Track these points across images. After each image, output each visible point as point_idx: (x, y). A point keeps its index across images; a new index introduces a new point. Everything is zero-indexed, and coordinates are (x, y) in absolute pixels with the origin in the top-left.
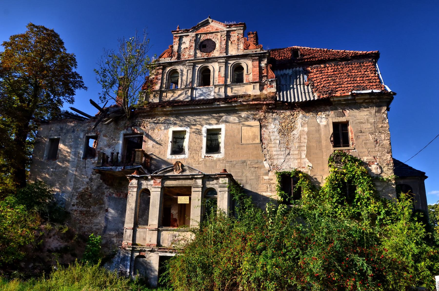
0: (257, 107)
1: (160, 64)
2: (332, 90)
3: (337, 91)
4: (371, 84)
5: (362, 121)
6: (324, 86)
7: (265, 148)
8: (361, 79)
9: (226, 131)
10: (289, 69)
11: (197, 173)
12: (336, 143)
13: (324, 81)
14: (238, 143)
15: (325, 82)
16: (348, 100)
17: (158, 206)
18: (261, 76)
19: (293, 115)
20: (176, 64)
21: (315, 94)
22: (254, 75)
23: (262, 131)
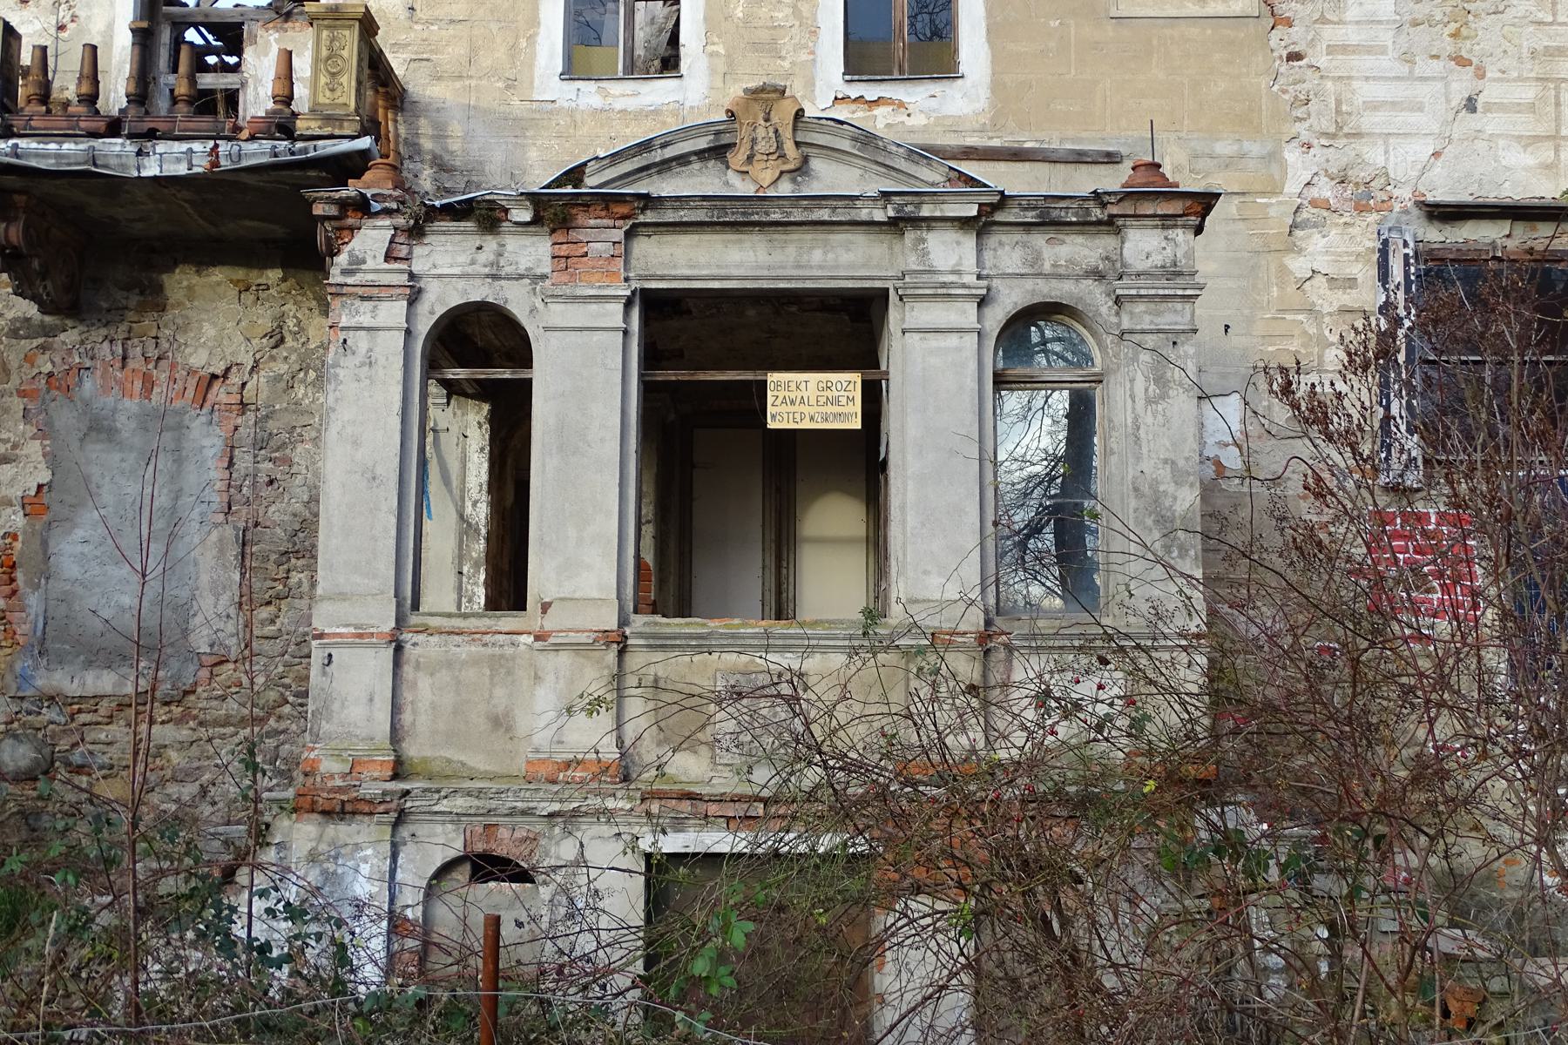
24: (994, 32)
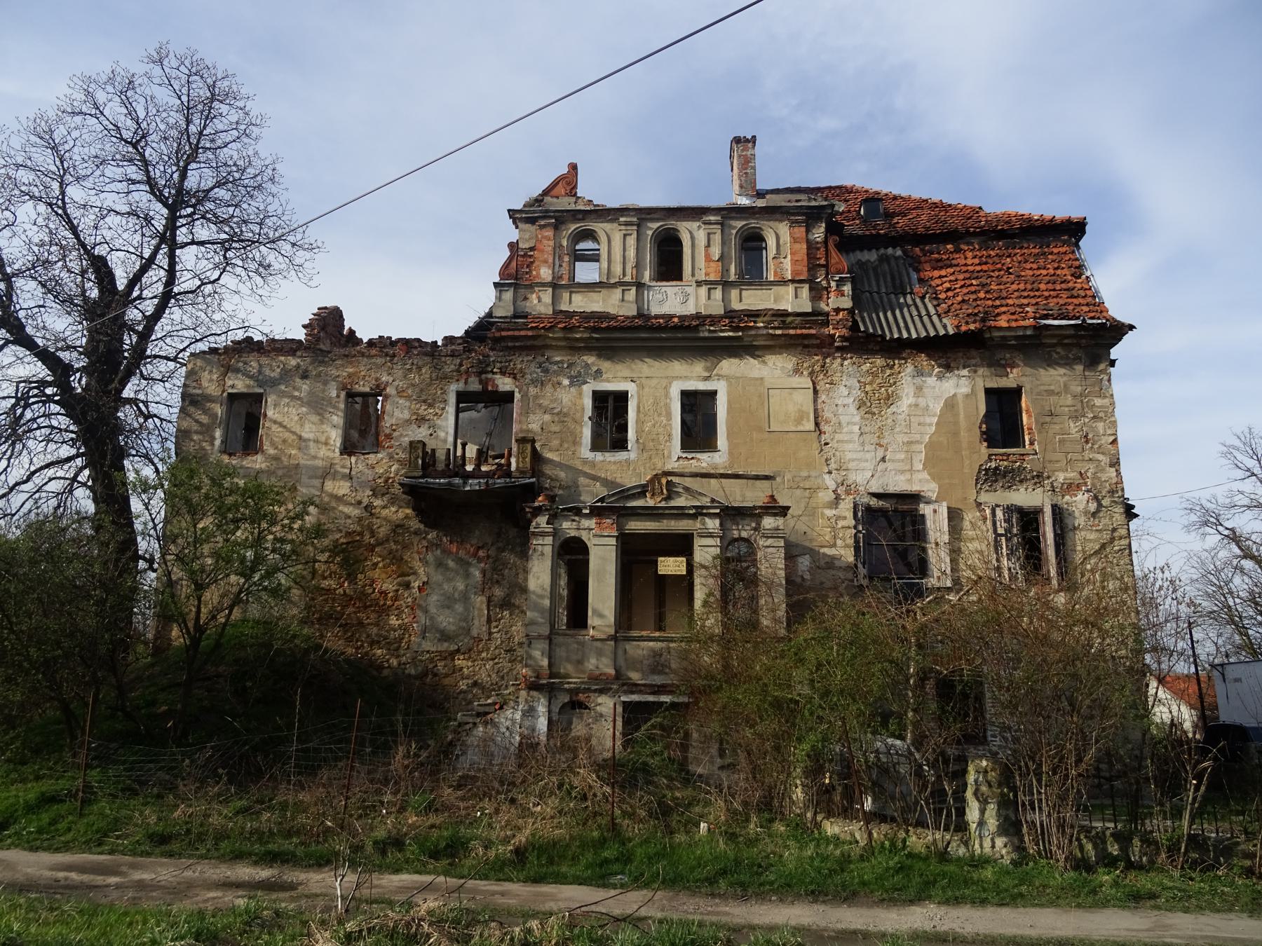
0: (806, 342)
1: (547, 211)
2: (986, 313)
3: (998, 315)
4: (1076, 301)
5: (1052, 388)
6: (963, 301)
7: (826, 444)
8: (1050, 286)
9: (729, 394)
10: (870, 250)
11: (705, 501)
12: (991, 439)
13: (962, 287)
14: (760, 429)
15: (965, 290)
16: (1025, 337)
17: (613, 581)
18: (813, 268)
19: (892, 367)
20: (593, 216)
21: (945, 320)
22: (794, 262)
23: (819, 401)
24: (730, 436)
